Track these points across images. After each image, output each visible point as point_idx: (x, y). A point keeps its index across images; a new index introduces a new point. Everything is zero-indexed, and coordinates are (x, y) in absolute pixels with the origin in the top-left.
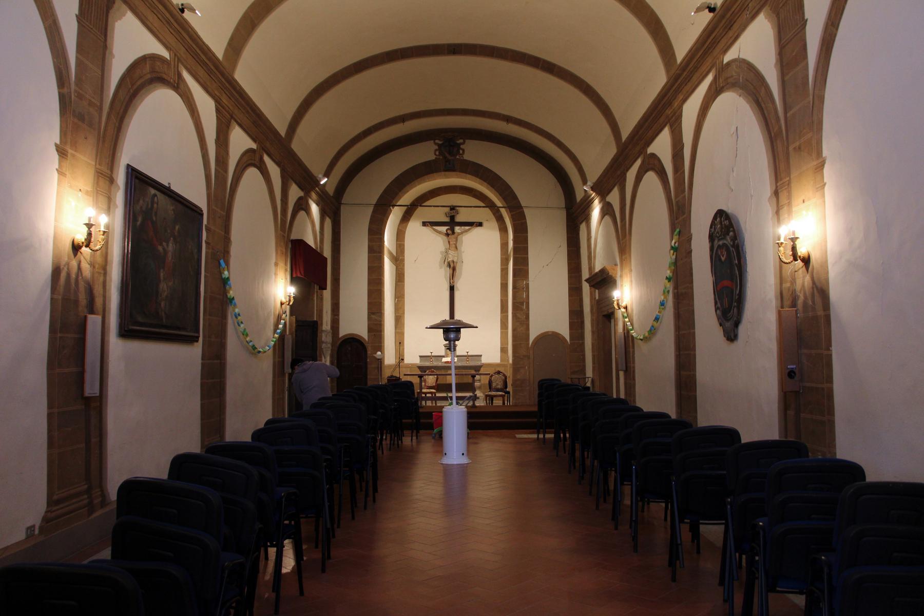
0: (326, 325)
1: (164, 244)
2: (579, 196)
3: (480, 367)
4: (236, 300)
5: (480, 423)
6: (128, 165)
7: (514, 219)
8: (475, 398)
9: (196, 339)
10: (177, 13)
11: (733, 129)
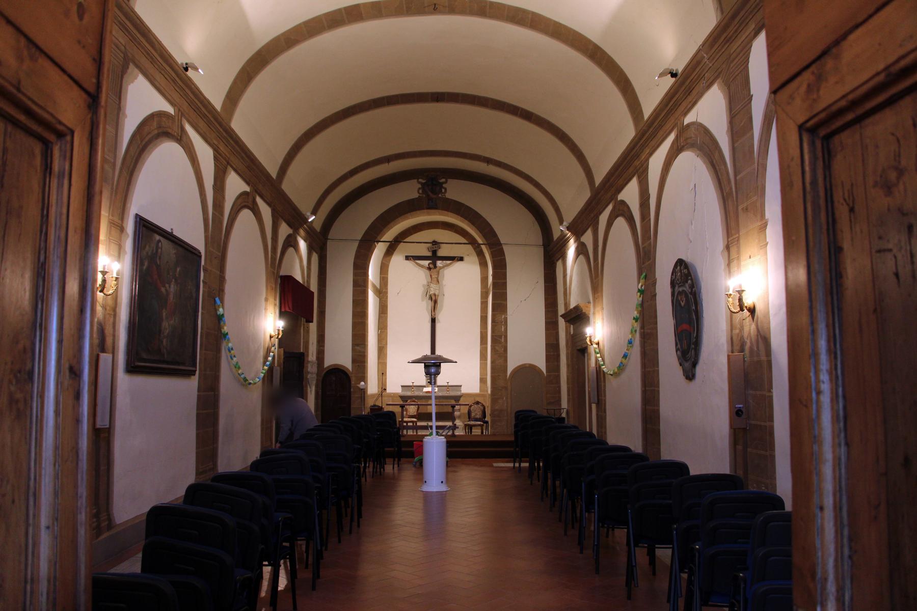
0: (312, 356)
1: (167, 285)
2: (556, 235)
3: (460, 397)
4: (229, 336)
5: (458, 451)
6: (137, 215)
7: (493, 256)
8: (455, 427)
9: (192, 373)
10: (181, 71)
11: (692, 186)
